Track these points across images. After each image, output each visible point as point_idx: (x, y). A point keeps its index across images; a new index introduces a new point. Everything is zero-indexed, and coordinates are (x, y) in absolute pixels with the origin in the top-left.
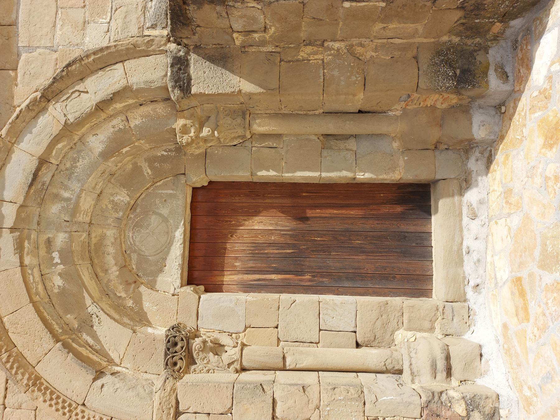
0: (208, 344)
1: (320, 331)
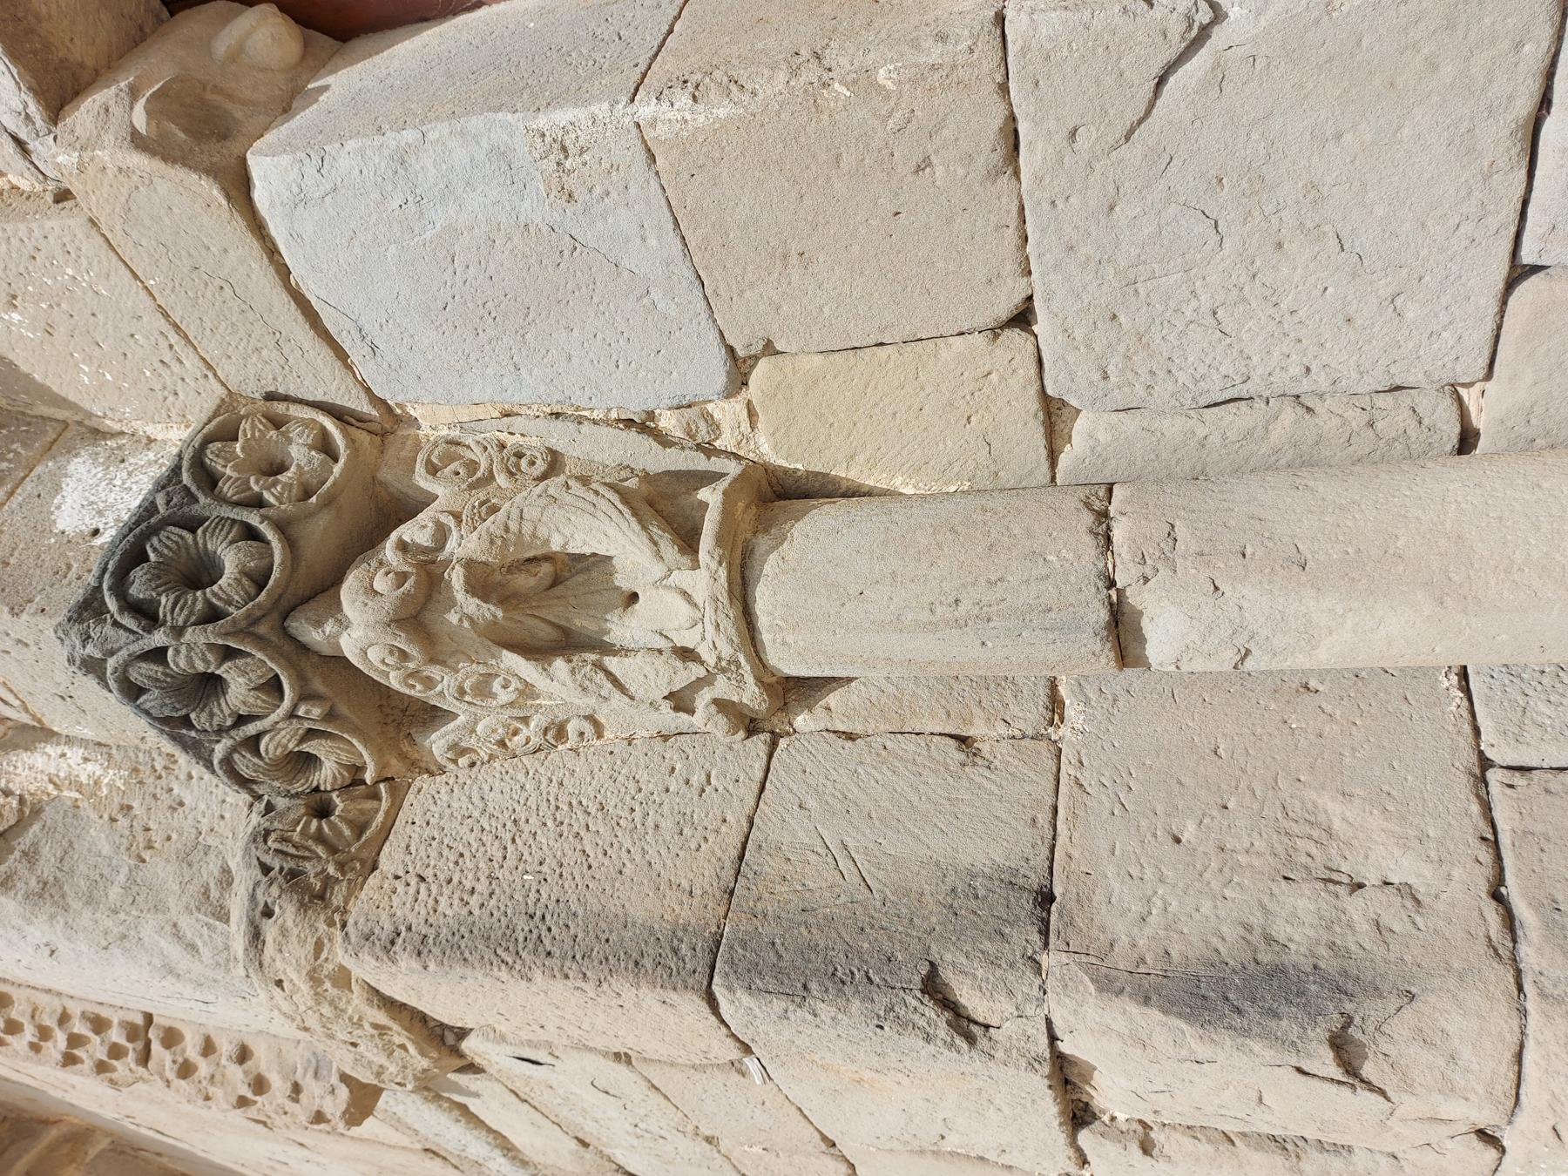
0: (453, 618)
1: (1510, 285)
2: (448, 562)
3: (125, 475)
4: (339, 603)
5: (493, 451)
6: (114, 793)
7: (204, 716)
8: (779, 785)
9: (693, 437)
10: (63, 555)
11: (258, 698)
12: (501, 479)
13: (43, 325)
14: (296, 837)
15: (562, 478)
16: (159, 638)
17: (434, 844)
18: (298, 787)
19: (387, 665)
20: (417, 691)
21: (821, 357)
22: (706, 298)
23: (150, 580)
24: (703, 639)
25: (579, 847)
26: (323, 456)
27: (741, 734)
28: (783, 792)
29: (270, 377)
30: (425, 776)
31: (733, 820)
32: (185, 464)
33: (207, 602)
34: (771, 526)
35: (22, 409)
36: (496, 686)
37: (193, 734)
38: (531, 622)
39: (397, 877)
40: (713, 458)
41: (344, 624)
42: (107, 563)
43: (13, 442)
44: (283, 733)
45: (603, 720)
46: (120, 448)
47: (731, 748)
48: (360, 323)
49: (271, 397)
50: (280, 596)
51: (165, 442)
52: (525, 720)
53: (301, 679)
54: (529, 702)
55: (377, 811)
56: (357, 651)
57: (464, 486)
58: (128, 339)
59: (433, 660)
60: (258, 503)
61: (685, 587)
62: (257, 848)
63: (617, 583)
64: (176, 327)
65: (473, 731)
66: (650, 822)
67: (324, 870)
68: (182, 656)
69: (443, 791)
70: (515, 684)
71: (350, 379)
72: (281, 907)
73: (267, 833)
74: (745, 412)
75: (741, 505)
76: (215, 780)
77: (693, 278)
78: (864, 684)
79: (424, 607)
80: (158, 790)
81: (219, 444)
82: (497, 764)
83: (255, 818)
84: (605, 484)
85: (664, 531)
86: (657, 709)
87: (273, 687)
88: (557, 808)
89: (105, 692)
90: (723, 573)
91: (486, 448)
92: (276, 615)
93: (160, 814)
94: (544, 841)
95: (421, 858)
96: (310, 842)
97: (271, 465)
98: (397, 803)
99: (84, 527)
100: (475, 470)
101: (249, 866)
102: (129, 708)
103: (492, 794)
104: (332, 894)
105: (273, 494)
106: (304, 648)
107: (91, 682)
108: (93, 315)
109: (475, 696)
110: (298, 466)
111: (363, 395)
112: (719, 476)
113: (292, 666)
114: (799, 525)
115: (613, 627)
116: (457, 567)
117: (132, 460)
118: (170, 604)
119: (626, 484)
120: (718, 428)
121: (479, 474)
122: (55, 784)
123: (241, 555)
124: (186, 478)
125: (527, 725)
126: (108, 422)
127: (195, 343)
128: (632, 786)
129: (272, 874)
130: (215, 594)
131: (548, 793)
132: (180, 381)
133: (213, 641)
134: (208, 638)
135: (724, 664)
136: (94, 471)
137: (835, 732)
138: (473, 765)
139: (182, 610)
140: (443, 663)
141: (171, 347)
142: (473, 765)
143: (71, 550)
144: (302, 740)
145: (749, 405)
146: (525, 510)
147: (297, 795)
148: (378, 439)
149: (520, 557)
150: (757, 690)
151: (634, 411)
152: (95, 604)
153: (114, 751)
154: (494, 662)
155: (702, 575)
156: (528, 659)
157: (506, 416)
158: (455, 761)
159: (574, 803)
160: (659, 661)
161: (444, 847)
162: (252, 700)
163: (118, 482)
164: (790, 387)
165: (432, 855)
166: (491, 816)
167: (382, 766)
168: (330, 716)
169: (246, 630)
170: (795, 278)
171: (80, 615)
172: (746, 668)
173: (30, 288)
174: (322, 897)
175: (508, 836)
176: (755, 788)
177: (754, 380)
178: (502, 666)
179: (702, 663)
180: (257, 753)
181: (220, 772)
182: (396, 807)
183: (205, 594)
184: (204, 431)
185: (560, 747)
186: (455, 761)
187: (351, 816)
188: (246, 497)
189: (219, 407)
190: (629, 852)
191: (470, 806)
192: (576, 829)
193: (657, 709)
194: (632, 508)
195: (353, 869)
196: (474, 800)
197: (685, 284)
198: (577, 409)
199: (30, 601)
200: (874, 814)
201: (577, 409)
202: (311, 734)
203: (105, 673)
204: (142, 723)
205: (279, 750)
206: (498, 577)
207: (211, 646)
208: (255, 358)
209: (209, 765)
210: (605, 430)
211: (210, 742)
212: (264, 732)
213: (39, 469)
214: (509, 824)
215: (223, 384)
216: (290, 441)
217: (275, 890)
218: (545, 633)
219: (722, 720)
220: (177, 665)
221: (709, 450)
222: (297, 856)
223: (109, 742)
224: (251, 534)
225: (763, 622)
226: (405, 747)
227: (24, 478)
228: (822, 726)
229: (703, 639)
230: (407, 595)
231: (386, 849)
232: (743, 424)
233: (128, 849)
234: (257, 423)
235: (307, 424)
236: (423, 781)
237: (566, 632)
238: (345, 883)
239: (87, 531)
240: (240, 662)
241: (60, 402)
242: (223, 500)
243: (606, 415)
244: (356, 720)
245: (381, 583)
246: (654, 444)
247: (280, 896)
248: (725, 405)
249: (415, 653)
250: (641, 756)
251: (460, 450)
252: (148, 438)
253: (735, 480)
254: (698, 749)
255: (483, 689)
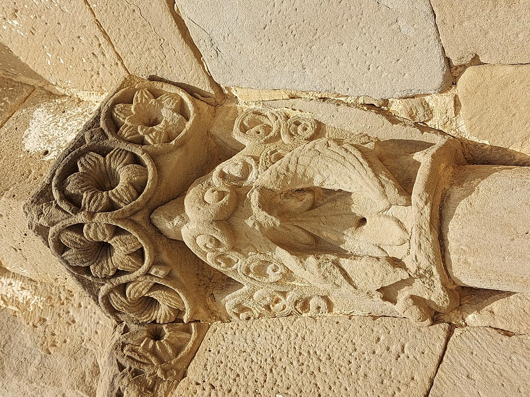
0: (250, 222)
2: (249, 188)
3: (64, 120)
4: (183, 207)
5: (281, 120)
6: (37, 310)
7: (98, 268)
8: (453, 360)
9: (413, 118)
10: (27, 164)
11: (130, 260)
12: (285, 138)
13: (30, 28)
14: (140, 350)
15: (324, 140)
16: (80, 218)
17: (222, 365)
18: (144, 319)
19: (207, 248)
20: (221, 267)
21: (513, 67)
22: (436, 25)
23: (78, 183)
24: (408, 253)
25: (313, 381)
26: (181, 116)
27: (428, 322)
28: (456, 364)
29: (154, 66)
30: (219, 322)
31: (418, 379)
32: (102, 115)
33: (109, 198)
34: (463, 181)
35: (10, 77)
36: (269, 269)
37: (90, 278)
38: (296, 230)
39: (198, 384)
40: (425, 133)
41: (185, 220)
42: (55, 170)
43: (4, 96)
44: (141, 284)
45: (333, 301)
46: (62, 104)
47: (419, 330)
48: (211, 35)
49: (152, 78)
50: (150, 199)
51: (88, 102)
52: (284, 294)
53: (156, 252)
54: (288, 283)
55: (189, 340)
56: (191, 238)
57: (262, 141)
58: (76, 39)
59: (234, 248)
60: (141, 142)
61: (398, 217)
62: (117, 354)
63: (353, 211)
64: (104, 33)
65: (251, 297)
66: (361, 372)
67: (155, 373)
68: (92, 230)
69: (229, 333)
70: (281, 269)
71: (200, 70)
72: (128, 392)
73: (124, 345)
74: (452, 103)
75: (443, 165)
76: (97, 308)
77: (429, 12)
78: (520, 298)
79: (233, 214)
80: (61, 312)
81: (122, 105)
82: (263, 320)
83: (117, 335)
84: (352, 145)
85: (389, 178)
86: (371, 297)
87: (139, 254)
88: (300, 354)
89: (46, 247)
90: (427, 210)
91: (277, 118)
92: (146, 210)
93: (61, 326)
94: (290, 374)
95: (213, 374)
96: (148, 354)
97: (150, 120)
98: (201, 337)
99: (40, 149)
100: (270, 131)
101: (111, 364)
102: (57, 258)
103: (259, 339)
104: (158, 388)
105: (150, 137)
106: (159, 232)
107: (39, 240)
108: (59, 23)
109: (255, 274)
110: (166, 121)
111: (207, 80)
112: (430, 145)
113: (152, 243)
114: (485, 182)
115: (347, 239)
116: (255, 191)
117: (69, 112)
118: (88, 198)
119: (366, 146)
120: (431, 113)
121: (272, 134)
122: (4, 301)
123: (130, 172)
124: (102, 124)
125: (285, 297)
126: (57, 88)
127: (114, 44)
128: (350, 346)
129: (124, 371)
130: (114, 195)
131: (295, 343)
132: (102, 66)
133: (110, 223)
134: (107, 221)
135: (421, 272)
136: (47, 117)
137: (496, 329)
138: (248, 318)
139: (94, 202)
140: (240, 251)
141: (100, 45)
142: (248, 318)
143: (32, 162)
144: (149, 291)
145: (456, 97)
146: (300, 158)
147: (143, 324)
148: (213, 108)
149: (293, 188)
150: (442, 292)
151: (376, 99)
152: (47, 194)
153: (39, 285)
154: (270, 254)
155: (412, 211)
156: (292, 254)
157: (292, 98)
158: (238, 315)
159: (312, 352)
160: (377, 265)
161: (228, 368)
162: (126, 262)
163: (60, 124)
164: (487, 87)
165: (220, 372)
166: (258, 353)
167: (195, 312)
168: (169, 277)
169: (128, 219)
170: (501, 14)
171: (38, 200)
172: (437, 276)
173: (26, 6)
174: (152, 390)
175: (268, 368)
176: (436, 360)
177: (461, 82)
178: (275, 257)
179: (406, 269)
180: (124, 294)
181: (101, 304)
182: (200, 339)
183: (108, 194)
184: (114, 97)
185: (304, 315)
186: (238, 315)
187: (173, 341)
188: (135, 138)
189: (124, 83)
190: (346, 390)
191: (245, 345)
192: (312, 369)
193: (371, 297)
194: (369, 162)
195: (172, 375)
196: (248, 341)
197: (423, 15)
198: (338, 96)
199: (7, 190)
200: (522, 389)
201: (338, 96)
202: (156, 286)
203: (47, 236)
204: (62, 268)
205: (137, 294)
206: (278, 200)
207: (108, 225)
208: (147, 54)
209: (96, 299)
210: (354, 110)
211: (99, 284)
212: (130, 282)
213: (17, 113)
214: (269, 360)
215: (126, 69)
216: (162, 106)
217: (125, 381)
218: (304, 238)
219: (416, 310)
220: (88, 235)
221: (423, 128)
222: (139, 362)
223: (37, 280)
224: (136, 160)
225: (452, 246)
226: (209, 302)
227: (9, 118)
228: (487, 323)
229: (408, 253)
230: (224, 205)
231: (192, 365)
232: (449, 112)
233: (42, 345)
234: (144, 93)
235: (174, 96)
236: (217, 325)
237: (316, 239)
238: (166, 383)
239: (42, 151)
240: (123, 237)
241: (33, 74)
242: (121, 138)
243: (356, 101)
244: (183, 281)
245: (209, 197)
246: (386, 121)
247: (128, 385)
248: (439, 97)
249: (224, 243)
250: (357, 327)
251: (261, 118)
252: (79, 99)
253: (441, 148)
254: (396, 327)
255: (261, 271)
